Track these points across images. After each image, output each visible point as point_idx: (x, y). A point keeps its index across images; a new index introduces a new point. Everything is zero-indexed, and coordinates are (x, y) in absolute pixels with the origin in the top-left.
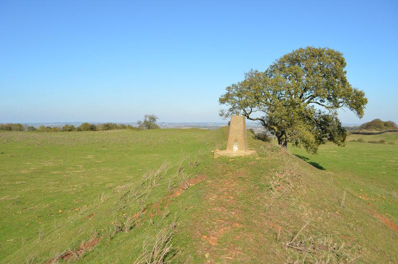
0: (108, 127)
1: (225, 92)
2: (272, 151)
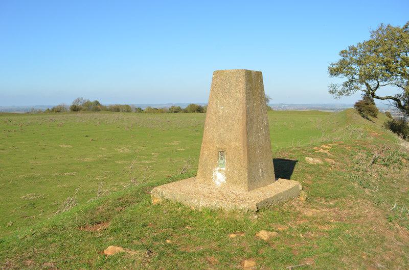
0: (117, 109)
1: (337, 58)
2: (386, 165)
